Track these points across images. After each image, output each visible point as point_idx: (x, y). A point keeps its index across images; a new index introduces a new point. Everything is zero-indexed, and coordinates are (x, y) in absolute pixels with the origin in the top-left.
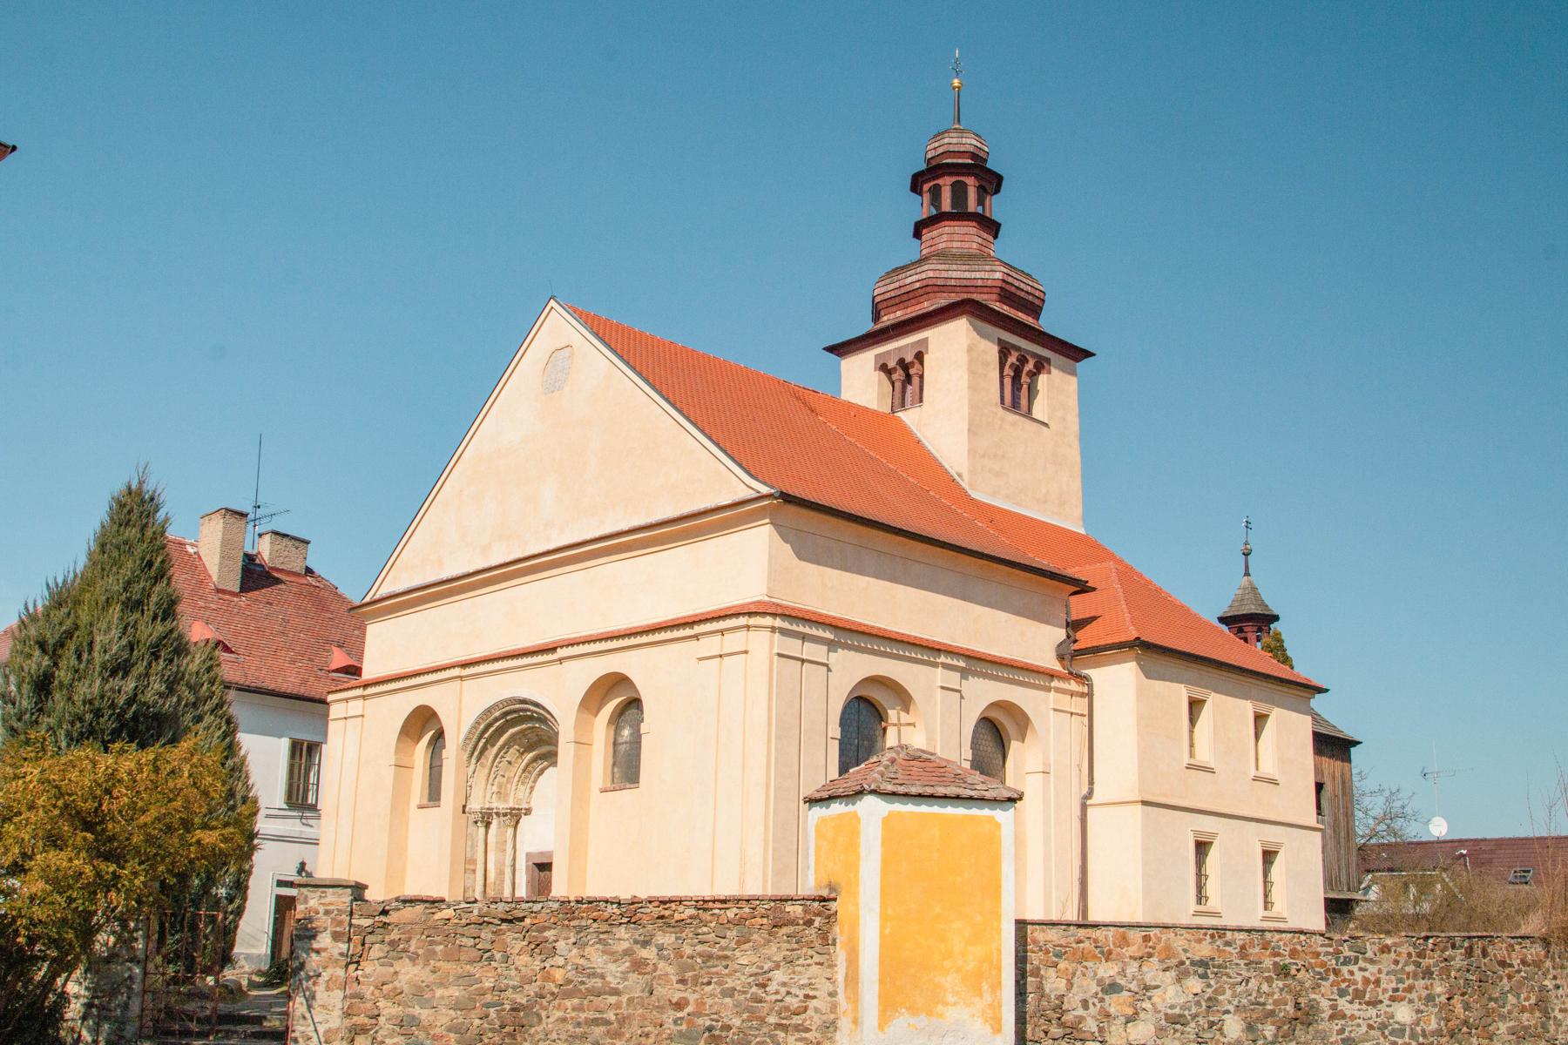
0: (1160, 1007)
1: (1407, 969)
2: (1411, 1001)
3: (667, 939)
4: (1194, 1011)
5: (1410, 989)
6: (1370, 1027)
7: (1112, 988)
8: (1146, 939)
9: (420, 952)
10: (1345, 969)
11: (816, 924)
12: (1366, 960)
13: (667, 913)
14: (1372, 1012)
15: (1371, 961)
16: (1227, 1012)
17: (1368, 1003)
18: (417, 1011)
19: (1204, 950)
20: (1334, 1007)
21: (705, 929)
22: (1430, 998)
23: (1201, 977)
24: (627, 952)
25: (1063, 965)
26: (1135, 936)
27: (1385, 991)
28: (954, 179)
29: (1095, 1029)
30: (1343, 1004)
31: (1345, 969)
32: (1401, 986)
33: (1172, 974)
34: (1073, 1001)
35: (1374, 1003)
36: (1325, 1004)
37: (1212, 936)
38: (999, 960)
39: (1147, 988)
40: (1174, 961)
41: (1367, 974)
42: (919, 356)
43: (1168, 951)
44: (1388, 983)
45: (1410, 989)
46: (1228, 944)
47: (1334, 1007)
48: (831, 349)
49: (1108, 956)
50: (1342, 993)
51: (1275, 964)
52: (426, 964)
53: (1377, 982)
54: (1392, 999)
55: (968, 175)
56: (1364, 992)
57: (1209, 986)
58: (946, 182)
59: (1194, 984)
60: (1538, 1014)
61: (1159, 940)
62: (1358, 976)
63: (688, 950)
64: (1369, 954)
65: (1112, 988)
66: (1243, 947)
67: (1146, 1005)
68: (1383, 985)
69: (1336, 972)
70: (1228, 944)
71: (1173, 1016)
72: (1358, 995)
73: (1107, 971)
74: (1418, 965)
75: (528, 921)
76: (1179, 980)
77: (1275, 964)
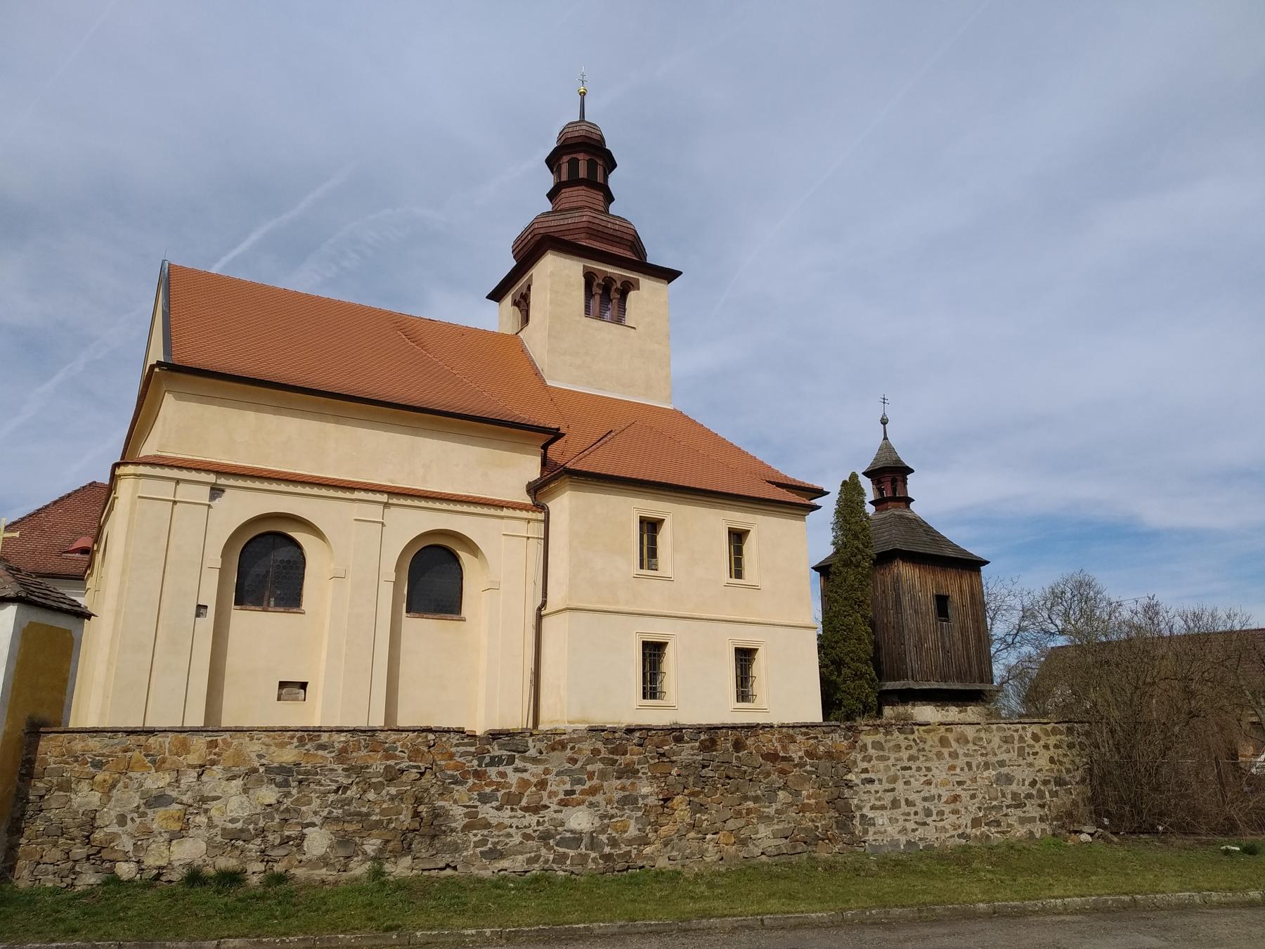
0: (218, 819)
5: (593, 791)
6: (527, 837)
7: (159, 800)
12: (525, 759)
14: (532, 819)
15: (535, 761)
16: (313, 825)
17: (526, 809)
20: (472, 814)
22: (629, 801)
27: (552, 794)
30: (487, 812)
31: (493, 772)
32: (578, 788)
34: (108, 817)
35: (536, 809)
36: (458, 811)
37: (301, 739)
41: (526, 776)
45: (593, 791)
49: (158, 765)
50: (484, 799)
53: (542, 784)
56: (521, 794)
59: (269, 794)
62: (513, 778)
64: (532, 752)
65: (159, 800)
67: (202, 819)
69: (478, 775)
70: (322, 747)
72: (512, 800)
73: (156, 781)
76: (246, 790)
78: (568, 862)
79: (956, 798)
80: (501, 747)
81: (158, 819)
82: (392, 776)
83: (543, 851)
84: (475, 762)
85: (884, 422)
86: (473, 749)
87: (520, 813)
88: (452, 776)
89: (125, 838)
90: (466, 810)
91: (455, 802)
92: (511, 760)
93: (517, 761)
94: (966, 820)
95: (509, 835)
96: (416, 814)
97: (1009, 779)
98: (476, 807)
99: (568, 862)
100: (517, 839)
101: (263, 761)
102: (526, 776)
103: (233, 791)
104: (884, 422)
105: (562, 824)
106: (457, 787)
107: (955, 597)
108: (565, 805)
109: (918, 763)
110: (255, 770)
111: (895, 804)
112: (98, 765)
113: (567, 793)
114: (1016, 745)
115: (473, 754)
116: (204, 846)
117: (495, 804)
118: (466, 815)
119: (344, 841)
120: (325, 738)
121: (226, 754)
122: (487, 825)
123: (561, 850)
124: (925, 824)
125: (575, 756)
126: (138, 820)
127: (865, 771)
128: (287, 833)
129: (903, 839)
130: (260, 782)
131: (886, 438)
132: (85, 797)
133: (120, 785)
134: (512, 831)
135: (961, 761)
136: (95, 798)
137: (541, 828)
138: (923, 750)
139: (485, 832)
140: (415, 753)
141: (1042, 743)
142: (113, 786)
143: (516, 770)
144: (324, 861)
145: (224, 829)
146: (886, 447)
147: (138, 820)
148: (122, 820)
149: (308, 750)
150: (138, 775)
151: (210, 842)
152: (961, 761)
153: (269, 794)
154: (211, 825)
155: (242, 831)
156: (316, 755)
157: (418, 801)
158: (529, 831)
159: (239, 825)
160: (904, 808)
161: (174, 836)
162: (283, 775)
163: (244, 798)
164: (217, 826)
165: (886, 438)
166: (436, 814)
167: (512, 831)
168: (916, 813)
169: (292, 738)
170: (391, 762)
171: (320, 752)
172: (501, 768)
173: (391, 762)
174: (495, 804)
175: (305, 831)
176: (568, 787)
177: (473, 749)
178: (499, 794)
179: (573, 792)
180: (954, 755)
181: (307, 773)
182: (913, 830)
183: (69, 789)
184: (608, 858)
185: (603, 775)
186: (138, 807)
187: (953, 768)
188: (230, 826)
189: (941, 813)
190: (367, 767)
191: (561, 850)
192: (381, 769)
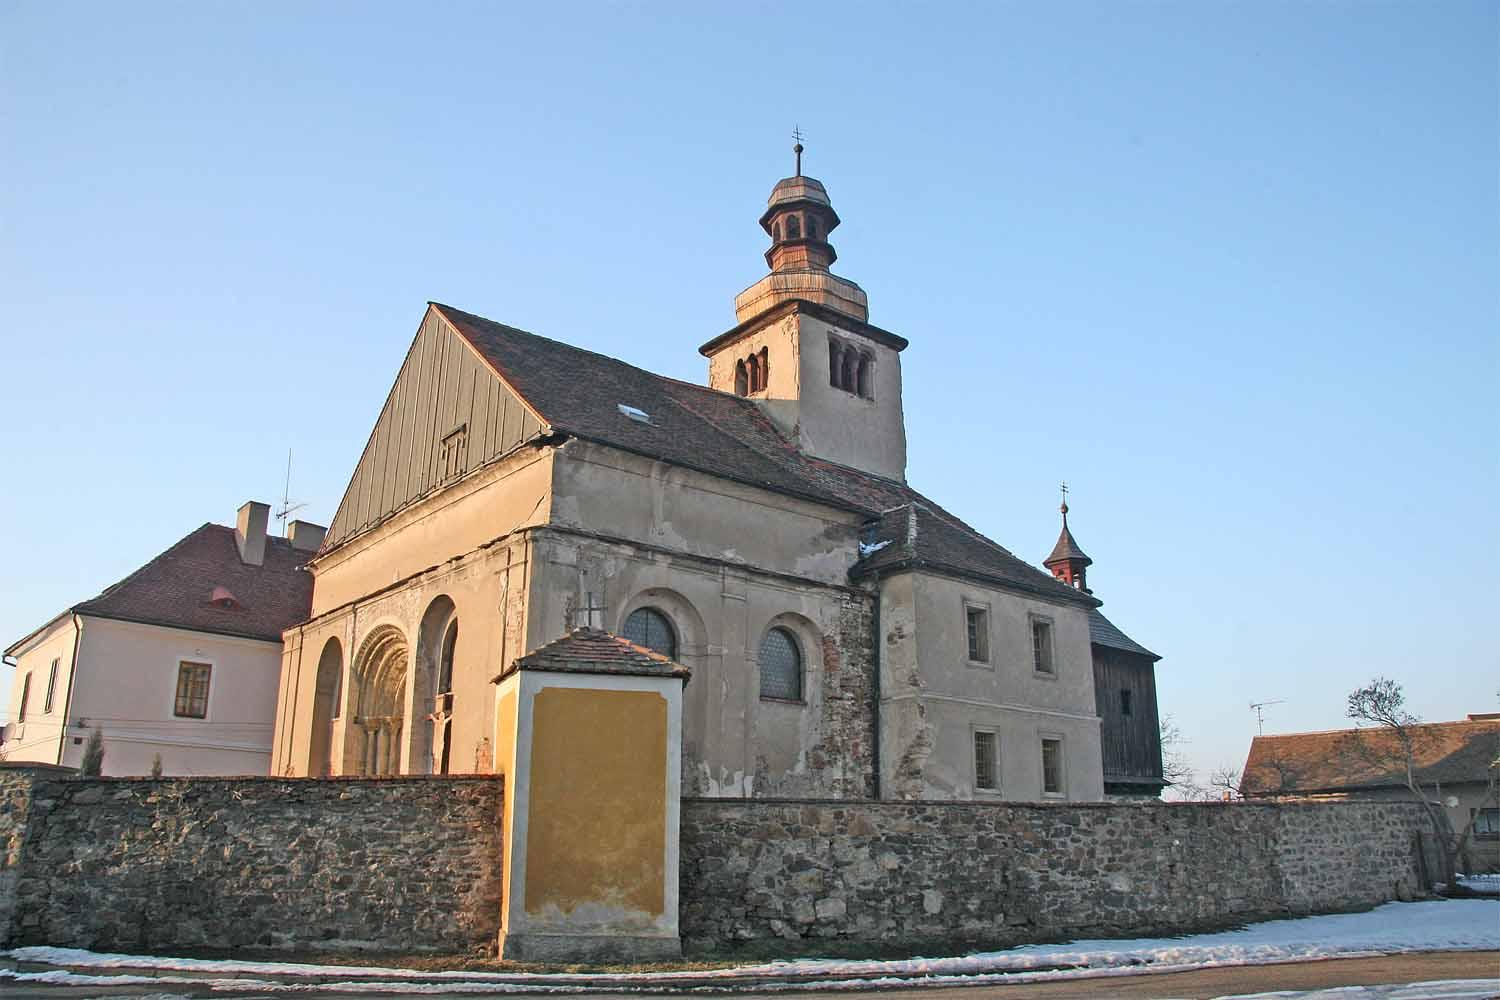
0: (853, 883)
1: (1124, 838)
2: (1128, 870)
3: (333, 819)
4: (889, 886)
5: (1128, 859)
6: (1084, 897)
7: (800, 865)
8: (838, 815)
9: (97, 831)
10: (1057, 841)
11: (482, 804)
12: (1079, 831)
13: (334, 793)
14: (1086, 882)
15: (1085, 832)
16: (928, 887)
17: (1082, 874)
18: (87, 888)
19: (904, 825)
20: (1044, 879)
21: (372, 809)
22: (1150, 866)
23: (898, 852)
24: (294, 833)
25: (746, 842)
26: (826, 814)
27: (1101, 861)
28: (786, 215)
29: (780, 907)
30: (1055, 876)
31: (1057, 841)
32: (1117, 856)
33: (866, 850)
34: (757, 878)
35: (1089, 873)
36: (1035, 875)
37: (910, 812)
38: (356, 948)
39: (838, 865)
40: (869, 838)
41: (1081, 845)
42: (765, 351)
43: (864, 828)
44: (1102, 854)
45: (1128, 859)
46: (929, 819)
47: (1044, 879)
48: (704, 350)
49: (796, 833)
50: (1053, 865)
51: (980, 838)
52: (102, 843)
53: (1092, 853)
54: (1108, 869)
55: (797, 210)
56: (1078, 861)
57: (906, 861)
58: (781, 219)
59: (891, 861)
60: (1268, 878)
61: (853, 816)
62: (1071, 847)
63: (353, 829)
64: (1083, 826)
65: (800, 865)
66: (945, 822)
67: (839, 883)
68: (1098, 855)
69: (1047, 844)
70: (929, 819)
71: (864, 892)
72: (1071, 866)
73: (795, 849)
74: (1135, 834)
75: (200, 800)
76: (873, 857)
77: (980, 838)
78: (1116, 918)
79: (1339, 865)
80: (1062, 821)
81: (802, 880)
82: (984, 845)
83: (1097, 909)
84: (1044, 833)
85: (1065, 509)
86: (1041, 822)
87: (1078, 877)
88: (1028, 846)
89: (775, 899)
90: (1041, 874)
91: (1032, 868)
92: (1068, 833)
93: (1073, 833)
94: (1346, 885)
95: (1072, 896)
96: (1005, 879)
97: (1369, 850)
98: (1047, 872)
99: (1116, 918)
100: (1078, 898)
101: (885, 831)
102: (1081, 845)
103: (862, 857)
104: (1065, 509)
105: (1109, 886)
106: (1032, 855)
107: (1135, 692)
108: (1109, 870)
109: (1316, 837)
110: (879, 839)
111: (1304, 871)
112: (743, 834)
113: (1110, 860)
114: (1371, 822)
115: (1041, 826)
116: (844, 905)
117: (1060, 869)
118: (1041, 879)
119: (951, 899)
120: (929, 812)
121: (852, 824)
122: (1056, 888)
123: (1111, 908)
124: (1323, 887)
125: (1113, 828)
126: (785, 883)
127: (1286, 843)
128: (910, 895)
129: (1311, 900)
130: (884, 849)
131: (1066, 527)
132: (737, 862)
133: (764, 851)
134: (1074, 892)
135: (1340, 836)
136: (744, 862)
137: (1094, 890)
138: (722, 828)
139: (1055, 893)
140: (999, 825)
141: (1385, 821)
142: (757, 853)
143: (1073, 840)
144: (939, 918)
145: (858, 891)
146: (1067, 539)
147: (785, 883)
148: (770, 882)
149: (917, 821)
150: (777, 842)
151: (848, 900)
152: (1340, 836)
153: (891, 861)
154: (847, 887)
155: (874, 892)
156: (924, 827)
157: (1005, 869)
158: (1086, 892)
159: (871, 887)
160: (1310, 874)
161: (822, 895)
162: (902, 844)
163: (872, 862)
164: (851, 888)
165: (1066, 527)
166: (1020, 876)
167: (1074, 892)
168: (1317, 878)
169: (903, 810)
170: (982, 833)
171: (928, 824)
172: (1062, 839)
173: (982, 833)
174: (1060, 869)
175: (923, 892)
176: (1110, 855)
177: (1041, 822)
178: (1063, 861)
179: (1114, 860)
180: (1336, 830)
181: (918, 841)
182: (1317, 892)
183: (720, 853)
184: (1141, 914)
185: (1133, 845)
186: (783, 870)
187: (1336, 841)
188: (862, 887)
189: (1331, 878)
190: (966, 837)
191: (1111, 908)
192: (975, 839)
